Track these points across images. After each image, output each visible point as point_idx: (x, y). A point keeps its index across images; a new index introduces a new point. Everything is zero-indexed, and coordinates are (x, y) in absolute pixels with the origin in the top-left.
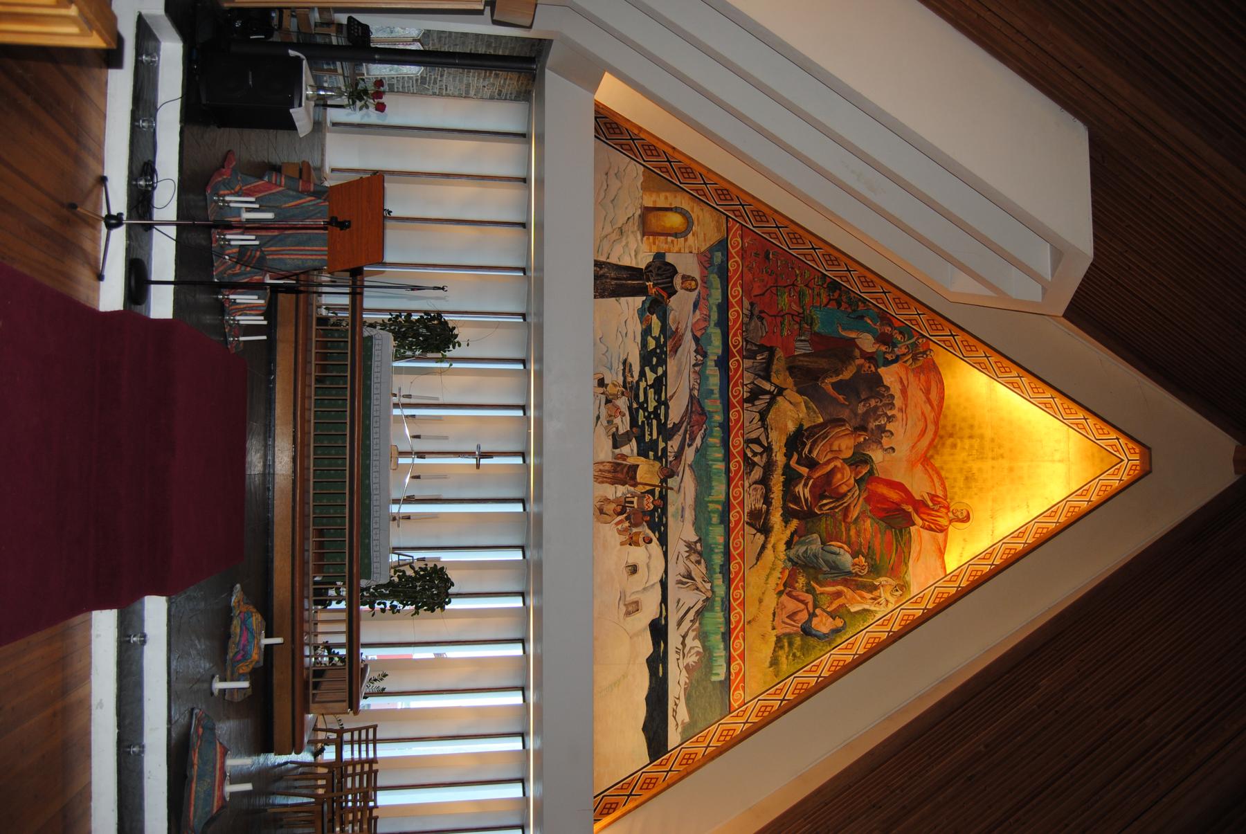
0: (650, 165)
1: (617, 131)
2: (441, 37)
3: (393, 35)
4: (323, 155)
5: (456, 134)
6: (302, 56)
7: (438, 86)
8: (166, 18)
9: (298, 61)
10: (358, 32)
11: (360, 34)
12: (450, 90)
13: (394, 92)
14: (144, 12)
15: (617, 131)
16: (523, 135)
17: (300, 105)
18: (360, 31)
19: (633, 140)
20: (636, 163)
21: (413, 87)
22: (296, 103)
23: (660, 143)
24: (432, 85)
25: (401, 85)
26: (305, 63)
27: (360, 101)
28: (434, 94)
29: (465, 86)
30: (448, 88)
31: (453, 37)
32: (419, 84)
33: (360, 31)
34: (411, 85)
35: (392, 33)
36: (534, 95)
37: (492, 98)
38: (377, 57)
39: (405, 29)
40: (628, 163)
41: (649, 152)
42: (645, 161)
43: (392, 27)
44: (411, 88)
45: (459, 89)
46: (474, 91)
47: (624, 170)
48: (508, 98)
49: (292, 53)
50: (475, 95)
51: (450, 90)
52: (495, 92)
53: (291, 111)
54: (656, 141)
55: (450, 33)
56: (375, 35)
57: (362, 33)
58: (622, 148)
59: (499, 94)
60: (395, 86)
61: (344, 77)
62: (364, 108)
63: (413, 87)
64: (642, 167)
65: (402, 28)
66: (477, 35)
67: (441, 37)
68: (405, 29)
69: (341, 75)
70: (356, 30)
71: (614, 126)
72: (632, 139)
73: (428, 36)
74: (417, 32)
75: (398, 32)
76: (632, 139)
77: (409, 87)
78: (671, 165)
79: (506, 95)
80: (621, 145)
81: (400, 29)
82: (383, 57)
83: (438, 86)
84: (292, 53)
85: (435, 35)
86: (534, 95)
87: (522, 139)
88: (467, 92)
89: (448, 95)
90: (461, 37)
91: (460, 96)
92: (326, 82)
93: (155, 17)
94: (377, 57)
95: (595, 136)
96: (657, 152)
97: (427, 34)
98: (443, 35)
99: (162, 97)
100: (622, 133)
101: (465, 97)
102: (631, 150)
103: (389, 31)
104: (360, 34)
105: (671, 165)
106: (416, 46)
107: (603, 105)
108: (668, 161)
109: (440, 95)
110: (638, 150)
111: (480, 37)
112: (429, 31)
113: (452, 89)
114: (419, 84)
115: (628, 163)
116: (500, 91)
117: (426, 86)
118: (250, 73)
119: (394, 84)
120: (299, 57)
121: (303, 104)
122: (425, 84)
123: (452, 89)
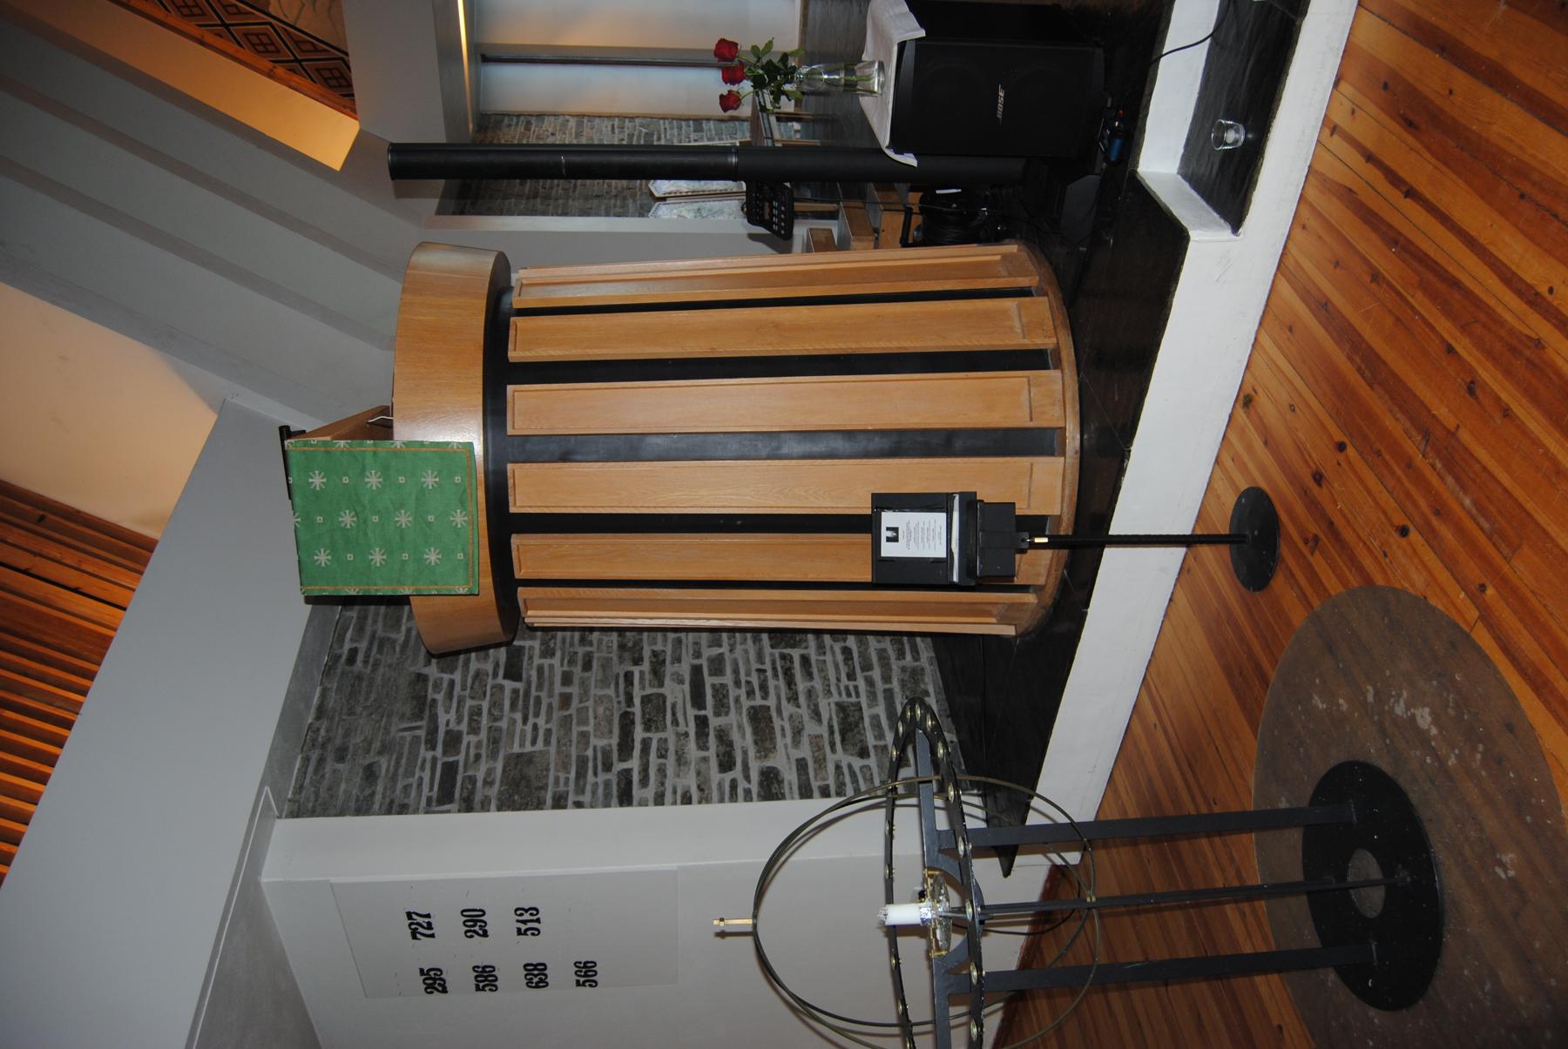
0: (334, 54)
1: (327, 74)
2: (622, 207)
3: (696, 206)
4: (805, 16)
5: (596, 56)
6: (890, 153)
7: (627, 131)
8: (1184, 223)
9: (898, 144)
10: (772, 207)
11: (767, 204)
12: (606, 127)
13: (694, 120)
14: (1226, 233)
15: (327, 74)
16: (486, 59)
17: (902, 46)
18: (767, 210)
19: (297, 60)
20: (282, 18)
21: (665, 129)
22: (910, 52)
23: (231, 51)
24: (636, 133)
25: (683, 132)
26: (884, 138)
27: (770, 62)
28: (632, 118)
29: (585, 133)
30: (610, 128)
31: (603, 207)
32: (656, 133)
33: (767, 210)
34: (668, 132)
35: (699, 209)
36: (471, 126)
37: (541, 116)
38: (734, 160)
39: (679, 216)
40: (298, 18)
41: (265, 40)
42: (270, 24)
43: (699, 218)
44: (667, 126)
45: (592, 128)
46: (569, 127)
47: (304, 5)
48: (515, 120)
49: (910, 160)
50: (568, 121)
51: (606, 127)
52: (537, 126)
53: (922, 33)
54: (237, 55)
55: (607, 214)
56: (733, 206)
57: (762, 208)
58: (312, 43)
59: (529, 123)
60: (692, 129)
61: (772, 138)
62: (761, 47)
63: (665, 129)
64: (273, 14)
65: (683, 217)
66: (565, 214)
67: (622, 207)
68: (679, 216)
69: (777, 141)
70: (775, 212)
71: (333, 82)
72: (299, 61)
73: (642, 208)
74: (660, 213)
75: (689, 211)
76: (299, 61)
77: (672, 128)
78: (220, 18)
79: (518, 122)
80: (316, 50)
81: (686, 215)
82: (720, 160)
83: (627, 131)
84: (910, 160)
85: (631, 210)
86: (471, 126)
87: (490, 54)
88: (580, 125)
89: (610, 117)
90: (591, 208)
91: (592, 117)
92: (796, 131)
93: (1203, 225)
94: (734, 160)
95: (347, 54)
96: (250, 42)
97: (643, 212)
98: (621, 210)
99: (1200, 55)
100: (318, 70)
101: (584, 116)
102: (296, 43)
103: (703, 212)
104: (767, 204)
105: (220, 18)
106: (662, 187)
107: (344, 113)
108: (227, 26)
109: (622, 117)
110: (284, 42)
111: (560, 211)
112: (641, 215)
113: (604, 128)
114: (656, 133)
115: (298, 18)
116: (527, 128)
117: (644, 130)
118: (999, 116)
119: (694, 132)
120: (896, 153)
121: (895, 49)
122: (646, 134)
123: (604, 128)
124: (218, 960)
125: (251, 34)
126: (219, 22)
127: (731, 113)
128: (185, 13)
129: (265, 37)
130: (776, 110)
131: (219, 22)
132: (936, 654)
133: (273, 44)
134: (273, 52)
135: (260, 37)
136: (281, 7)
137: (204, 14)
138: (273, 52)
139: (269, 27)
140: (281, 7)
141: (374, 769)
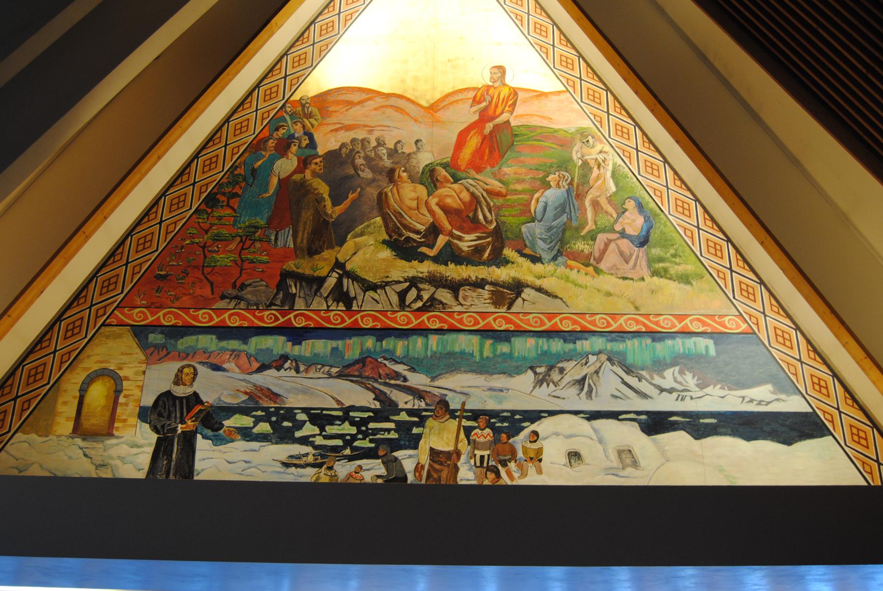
20: (12, 441)
40: (8, 453)
42: (9, 431)
78: (59, 350)
105: (59, 350)
115: (8, 453)
124: (861, 134)
125: (5, 416)
126: (19, 394)
127: (509, 311)
128: (264, 115)
129: (78, 331)
130: (271, 143)
131: (19, 394)
132: (341, 483)
133: (35, 381)
134: (28, 380)
135: (114, 284)
136: (19, 442)
137: (28, 385)
138: (28, 380)
139: (46, 382)
140: (19, 442)
141: (287, 136)
